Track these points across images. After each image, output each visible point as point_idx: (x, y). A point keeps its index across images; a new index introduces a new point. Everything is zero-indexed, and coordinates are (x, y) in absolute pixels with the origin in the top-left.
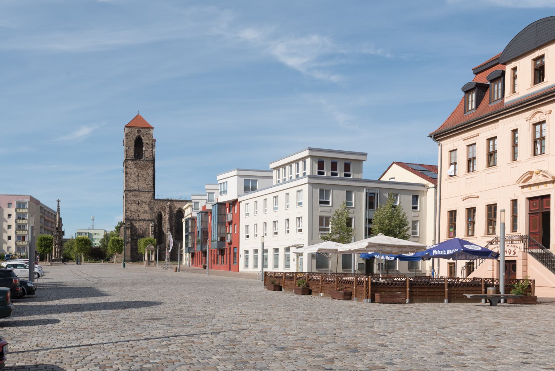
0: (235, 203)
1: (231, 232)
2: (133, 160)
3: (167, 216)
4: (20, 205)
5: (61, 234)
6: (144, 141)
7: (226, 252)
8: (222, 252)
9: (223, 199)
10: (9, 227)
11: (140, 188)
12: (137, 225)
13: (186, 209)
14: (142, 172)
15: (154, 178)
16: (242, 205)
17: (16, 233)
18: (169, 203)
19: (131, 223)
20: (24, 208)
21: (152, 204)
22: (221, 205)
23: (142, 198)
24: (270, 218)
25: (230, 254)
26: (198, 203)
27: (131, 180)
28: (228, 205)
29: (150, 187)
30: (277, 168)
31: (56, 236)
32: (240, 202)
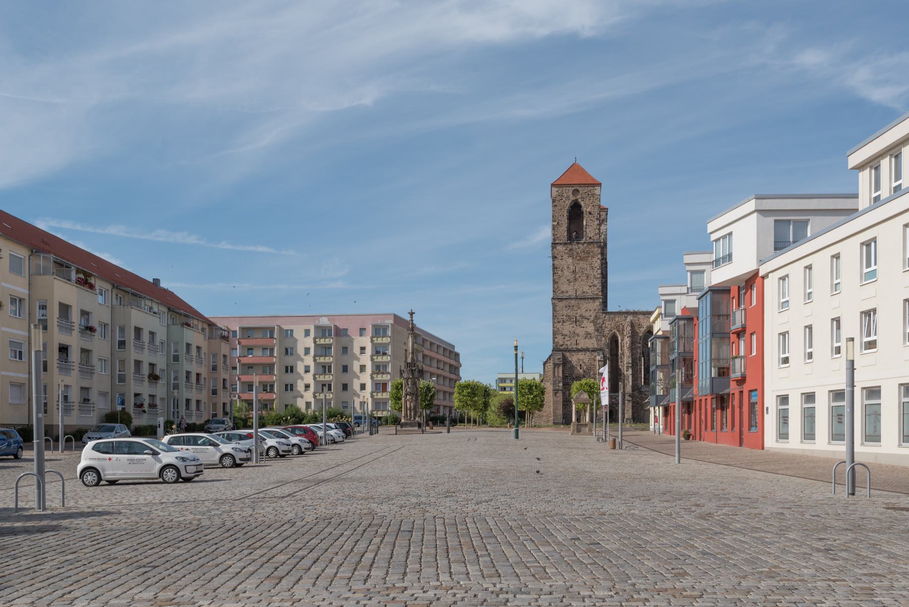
0: (752, 281)
1: (742, 353)
2: (565, 244)
3: (627, 341)
4: (379, 331)
5: (416, 374)
6: (584, 209)
7: (732, 403)
8: (722, 401)
9: (718, 276)
10: (363, 368)
11: (579, 293)
12: (574, 359)
13: (654, 322)
14: (582, 264)
15: (604, 276)
16: (771, 286)
17: (372, 378)
18: (629, 318)
19: (564, 356)
20: (385, 335)
21: (600, 321)
22: (720, 291)
23: (582, 312)
24: (851, 302)
25: (741, 407)
26: (673, 301)
27: (563, 280)
28: (734, 292)
29: (597, 290)
30: (873, 163)
31: (407, 379)
32: (763, 278)
